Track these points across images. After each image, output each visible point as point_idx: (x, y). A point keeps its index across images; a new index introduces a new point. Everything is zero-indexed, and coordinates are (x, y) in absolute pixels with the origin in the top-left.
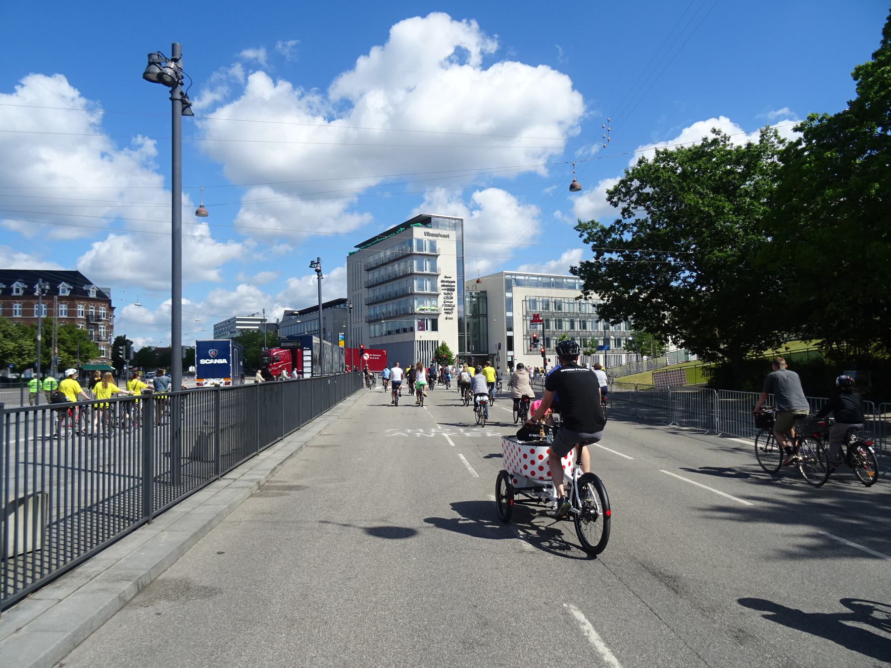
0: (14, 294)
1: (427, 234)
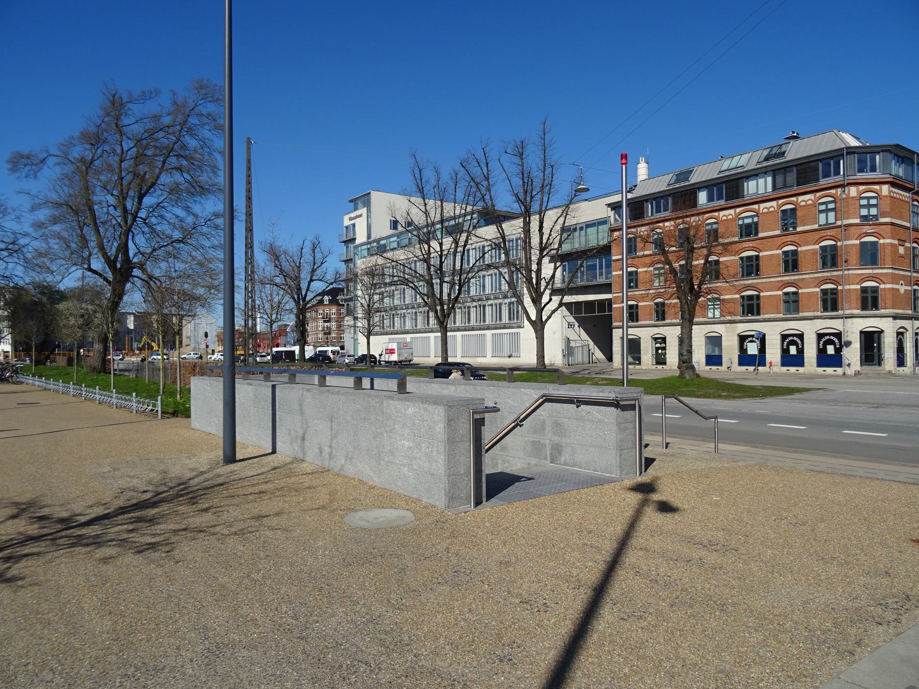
0: (325, 303)
1: (351, 219)
